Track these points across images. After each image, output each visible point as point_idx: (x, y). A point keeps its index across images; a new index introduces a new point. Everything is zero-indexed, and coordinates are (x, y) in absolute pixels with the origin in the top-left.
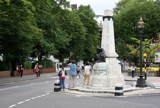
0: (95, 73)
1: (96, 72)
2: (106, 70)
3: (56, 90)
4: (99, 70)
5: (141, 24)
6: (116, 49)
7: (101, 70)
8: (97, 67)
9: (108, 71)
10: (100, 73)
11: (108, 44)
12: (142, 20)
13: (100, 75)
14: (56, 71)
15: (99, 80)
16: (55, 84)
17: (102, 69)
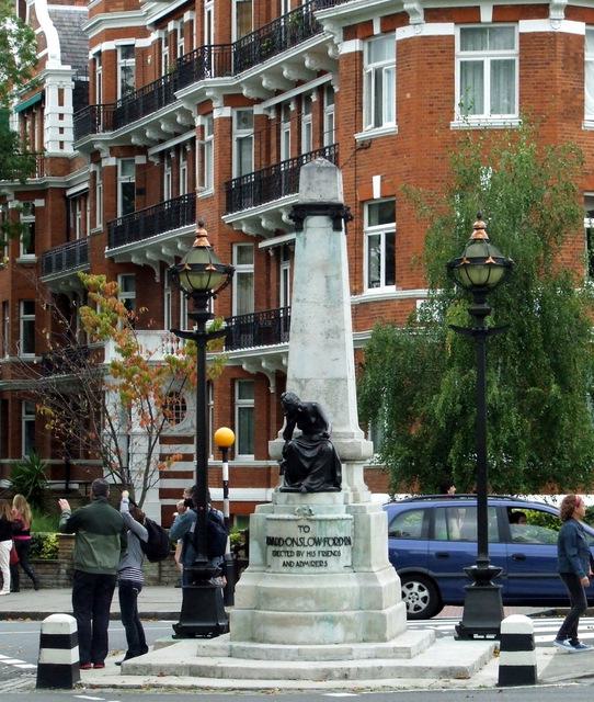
0: (287, 559)
1: (299, 554)
2: (352, 541)
3: (55, 677)
4: (317, 542)
5: (491, 260)
6: (359, 421)
7: (331, 542)
8: (301, 523)
9: (361, 544)
10: (324, 559)
11: (338, 380)
12: (484, 235)
13: (322, 569)
14: (369, 211)
15: (322, 599)
16: (268, 538)
17: (333, 532)
